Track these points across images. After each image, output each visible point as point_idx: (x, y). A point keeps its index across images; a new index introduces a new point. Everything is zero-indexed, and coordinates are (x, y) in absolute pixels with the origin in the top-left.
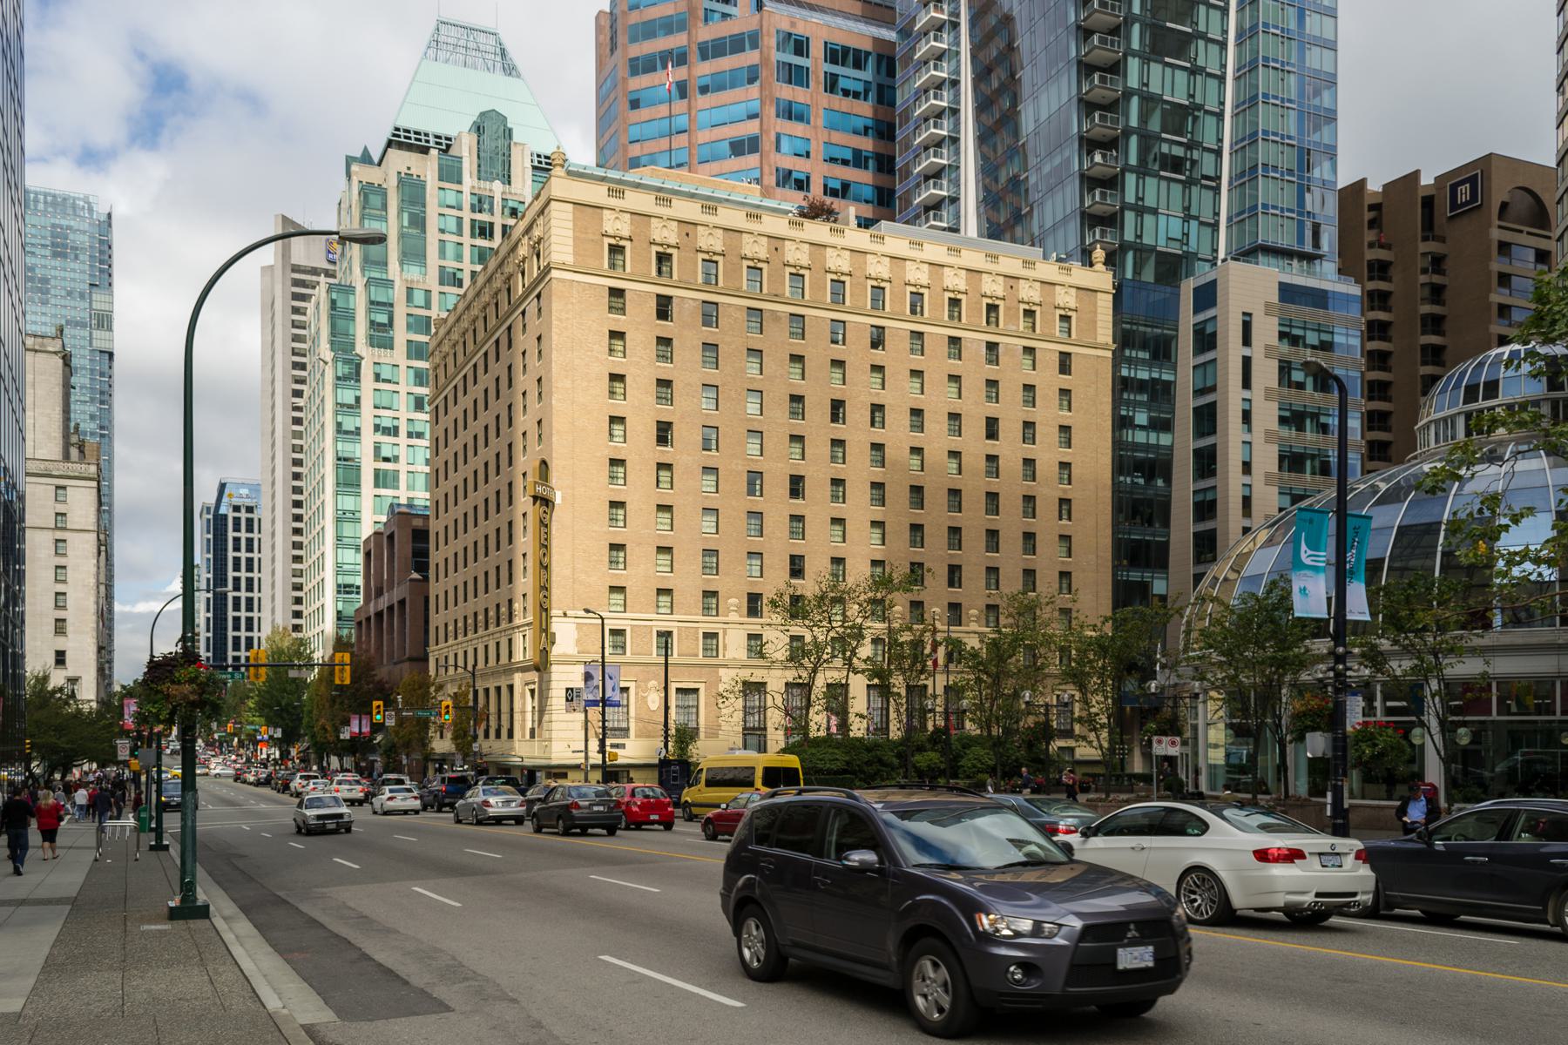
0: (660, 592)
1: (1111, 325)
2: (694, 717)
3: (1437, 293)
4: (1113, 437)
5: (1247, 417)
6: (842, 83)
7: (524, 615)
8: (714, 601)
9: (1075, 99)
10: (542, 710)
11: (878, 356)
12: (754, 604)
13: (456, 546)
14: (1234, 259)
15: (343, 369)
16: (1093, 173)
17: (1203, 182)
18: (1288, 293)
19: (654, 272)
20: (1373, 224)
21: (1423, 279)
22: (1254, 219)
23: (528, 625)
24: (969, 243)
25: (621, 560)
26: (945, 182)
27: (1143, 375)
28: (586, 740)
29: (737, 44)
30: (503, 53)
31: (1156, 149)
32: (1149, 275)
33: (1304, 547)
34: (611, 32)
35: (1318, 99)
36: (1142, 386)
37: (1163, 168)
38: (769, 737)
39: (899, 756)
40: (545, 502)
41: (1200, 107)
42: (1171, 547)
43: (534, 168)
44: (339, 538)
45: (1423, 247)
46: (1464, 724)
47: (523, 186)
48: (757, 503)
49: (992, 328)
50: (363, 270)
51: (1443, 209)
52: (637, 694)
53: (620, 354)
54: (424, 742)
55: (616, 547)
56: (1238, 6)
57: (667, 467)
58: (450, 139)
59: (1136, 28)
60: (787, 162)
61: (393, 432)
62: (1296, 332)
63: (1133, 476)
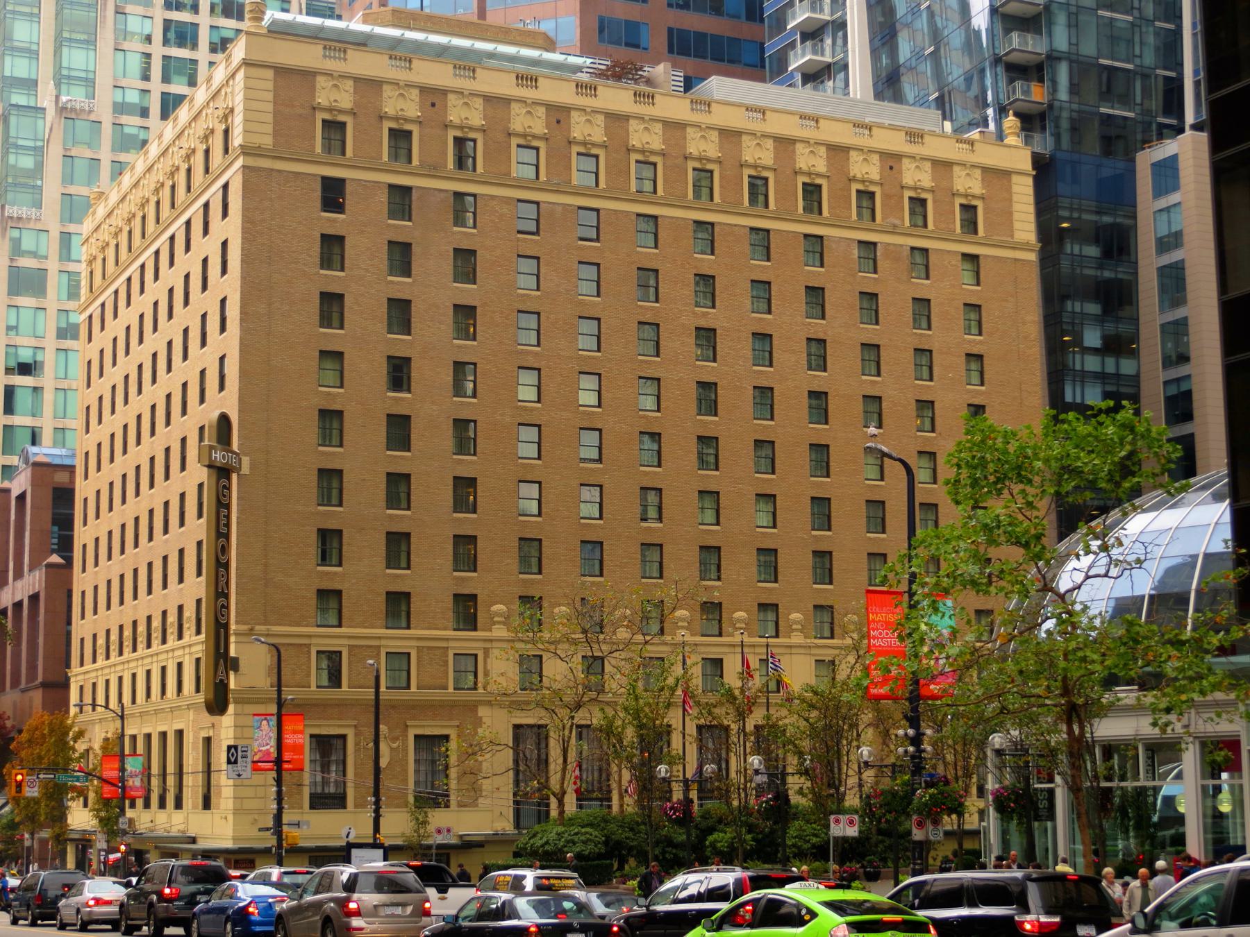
52: (357, 744)
54: (59, 816)
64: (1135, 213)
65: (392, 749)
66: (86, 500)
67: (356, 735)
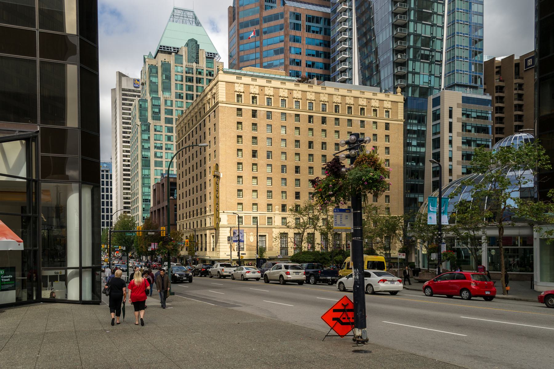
0: (254, 204)
1: (403, 111)
2: (265, 244)
3: (520, 97)
4: (404, 150)
5: (450, 142)
6: (312, 29)
7: (210, 211)
8: (271, 207)
9: (391, 36)
10: (216, 242)
11: (324, 126)
12: (284, 208)
13: (187, 189)
14: (445, 89)
15: (144, 128)
16: (398, 61)
17: (436, 62)
18: (466, 100)
19: (251, 103)
20: (498, 73)
21: (515, 92)
22: (454, 75)
23: (211, 215)
24: (356, 88)
25: (241, 194)
26: (347, 63)
27: (415, 128)
28: (231, 252)
29: (276, 17)
30: (196, 18)
31: (419, 53)
32: (417, 95)
33: (430, 206)
34: (233, 14)
35: (477, 32)
36: (414, 132)
37: (422, 59)
38: (289, 250)
39: (331, 257)
40: (217, 177)
41: (435, 37)
42: (425, 186)
43: (207, 57)
44: (143, 184)
45: (515, 81)
46: (493, 249)
47: (203, 64)
48: (285, 175)
49: (362, 116)
50: (150, 94)
51: (523, 68)
52: (246, 237)
53: (241, 129)
55: (239, 190)
56: (448, 2)
57: (256, 164)
58: (178, 49)
59: (412, 12)
60: (293, 56)
61: (161, 148)
62: (468, 113)
63: (411, 162)
64: (427, 111)
66: (180, 184)
67: (246, 235)
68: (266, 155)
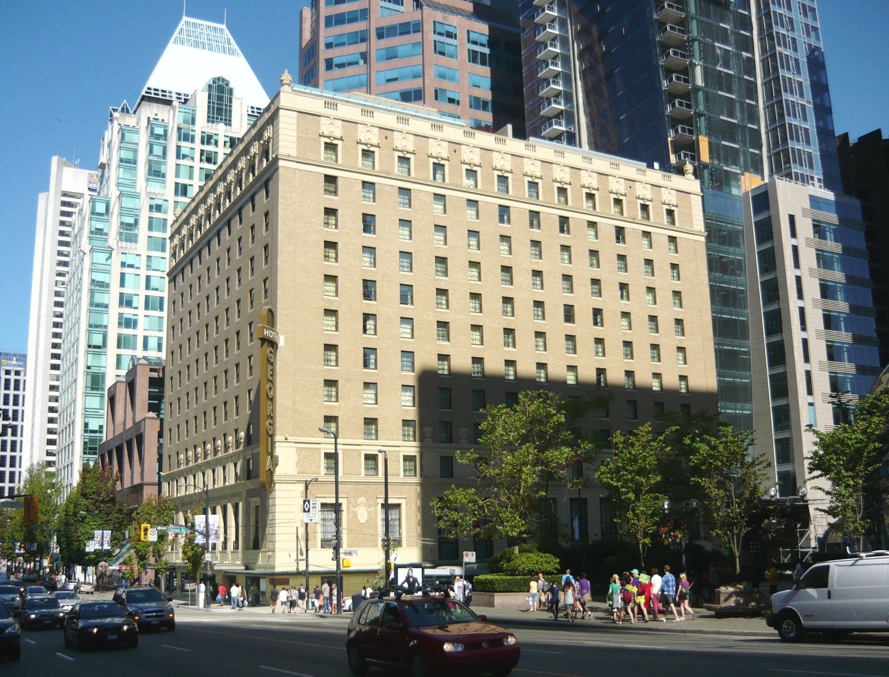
65: (368, 512)
67: (348, 503)
68: (398, 294)
